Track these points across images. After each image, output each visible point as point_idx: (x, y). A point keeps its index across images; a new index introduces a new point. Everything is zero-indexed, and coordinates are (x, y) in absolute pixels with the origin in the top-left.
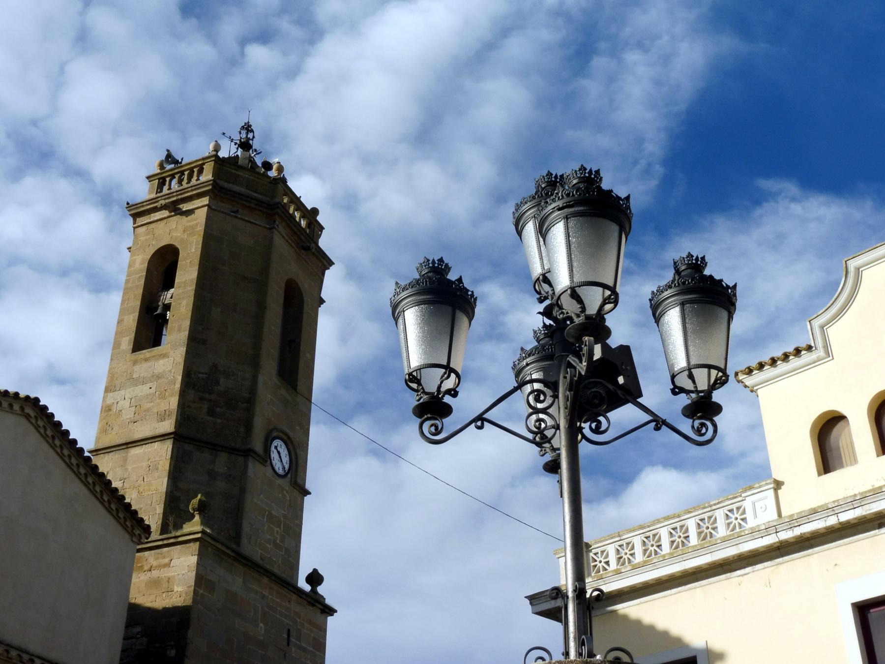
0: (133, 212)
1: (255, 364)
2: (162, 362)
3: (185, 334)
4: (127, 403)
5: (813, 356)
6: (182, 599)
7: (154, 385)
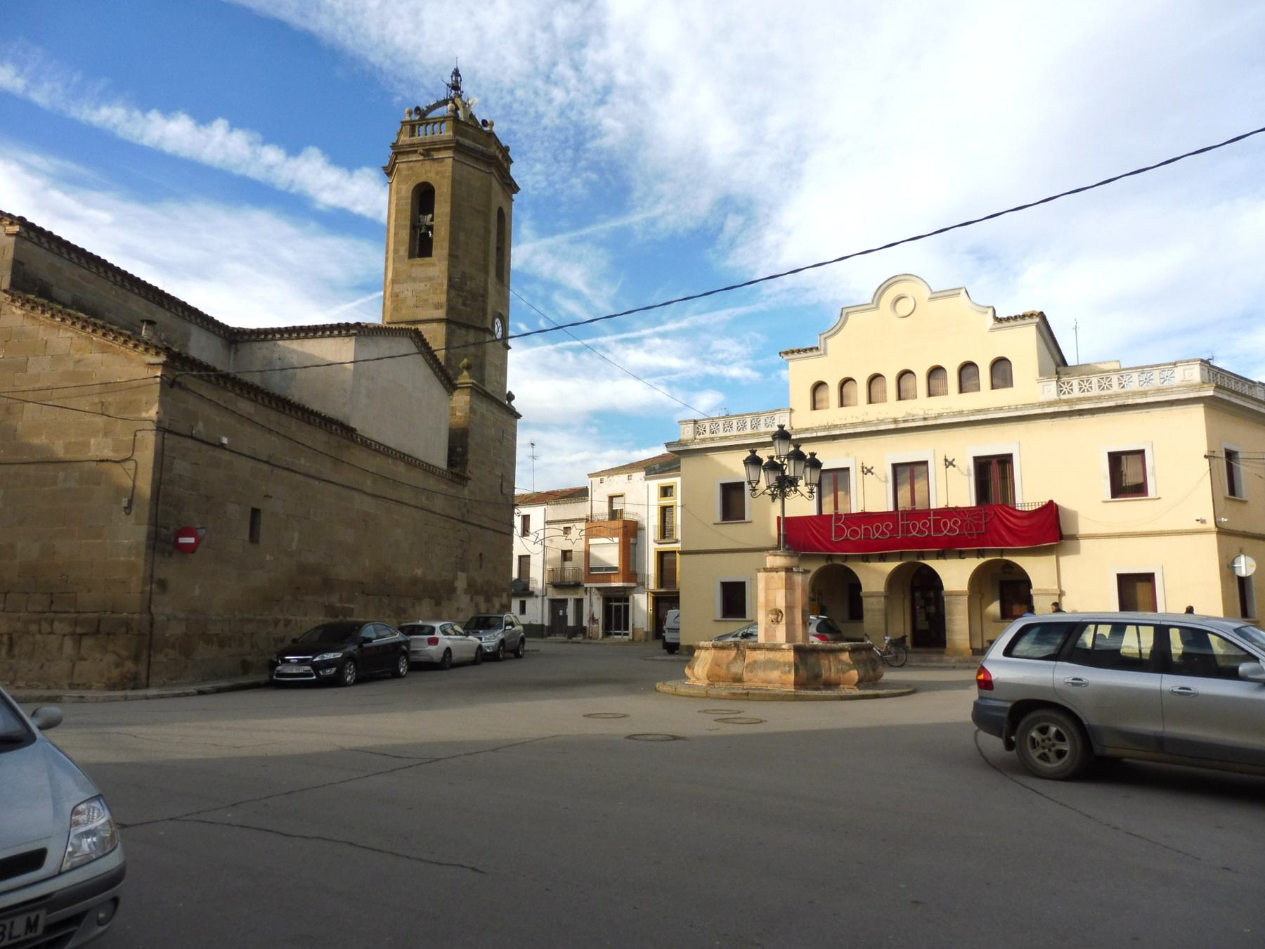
0: (396, 151)
1: (487, 272)
2: (431, 269)
3: (446, 252)
4: (409, 294)
5: (818, 353)
6: (462, 420)
7: (428, 284)
